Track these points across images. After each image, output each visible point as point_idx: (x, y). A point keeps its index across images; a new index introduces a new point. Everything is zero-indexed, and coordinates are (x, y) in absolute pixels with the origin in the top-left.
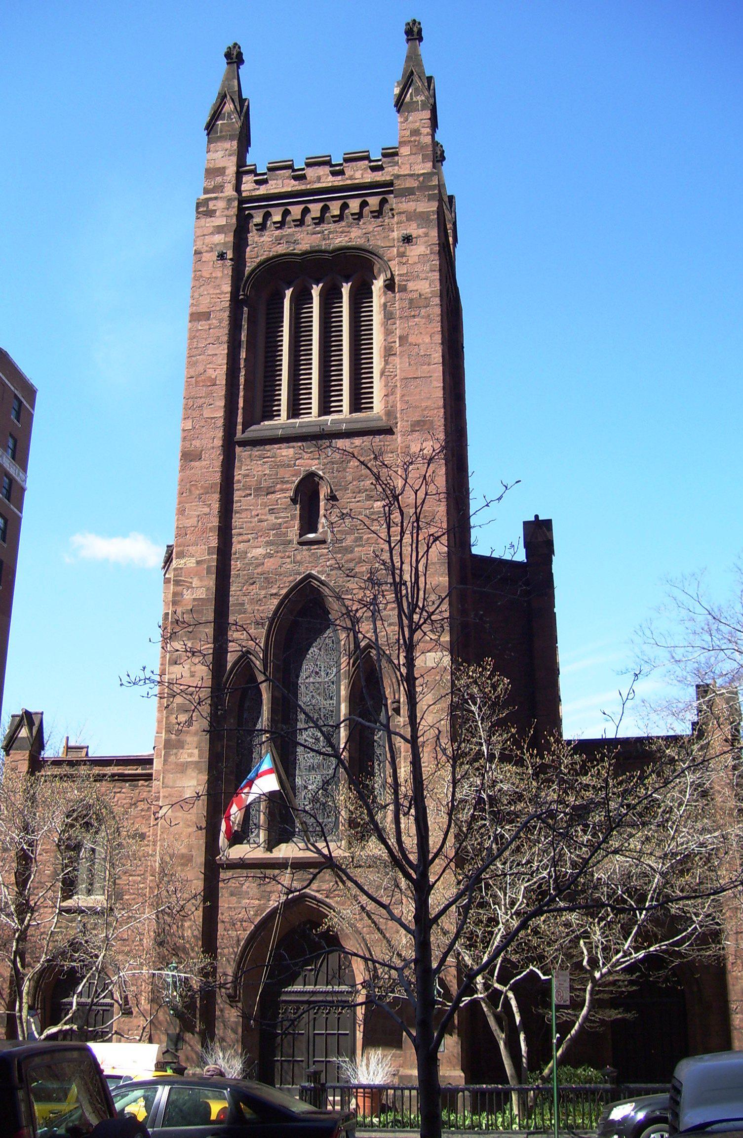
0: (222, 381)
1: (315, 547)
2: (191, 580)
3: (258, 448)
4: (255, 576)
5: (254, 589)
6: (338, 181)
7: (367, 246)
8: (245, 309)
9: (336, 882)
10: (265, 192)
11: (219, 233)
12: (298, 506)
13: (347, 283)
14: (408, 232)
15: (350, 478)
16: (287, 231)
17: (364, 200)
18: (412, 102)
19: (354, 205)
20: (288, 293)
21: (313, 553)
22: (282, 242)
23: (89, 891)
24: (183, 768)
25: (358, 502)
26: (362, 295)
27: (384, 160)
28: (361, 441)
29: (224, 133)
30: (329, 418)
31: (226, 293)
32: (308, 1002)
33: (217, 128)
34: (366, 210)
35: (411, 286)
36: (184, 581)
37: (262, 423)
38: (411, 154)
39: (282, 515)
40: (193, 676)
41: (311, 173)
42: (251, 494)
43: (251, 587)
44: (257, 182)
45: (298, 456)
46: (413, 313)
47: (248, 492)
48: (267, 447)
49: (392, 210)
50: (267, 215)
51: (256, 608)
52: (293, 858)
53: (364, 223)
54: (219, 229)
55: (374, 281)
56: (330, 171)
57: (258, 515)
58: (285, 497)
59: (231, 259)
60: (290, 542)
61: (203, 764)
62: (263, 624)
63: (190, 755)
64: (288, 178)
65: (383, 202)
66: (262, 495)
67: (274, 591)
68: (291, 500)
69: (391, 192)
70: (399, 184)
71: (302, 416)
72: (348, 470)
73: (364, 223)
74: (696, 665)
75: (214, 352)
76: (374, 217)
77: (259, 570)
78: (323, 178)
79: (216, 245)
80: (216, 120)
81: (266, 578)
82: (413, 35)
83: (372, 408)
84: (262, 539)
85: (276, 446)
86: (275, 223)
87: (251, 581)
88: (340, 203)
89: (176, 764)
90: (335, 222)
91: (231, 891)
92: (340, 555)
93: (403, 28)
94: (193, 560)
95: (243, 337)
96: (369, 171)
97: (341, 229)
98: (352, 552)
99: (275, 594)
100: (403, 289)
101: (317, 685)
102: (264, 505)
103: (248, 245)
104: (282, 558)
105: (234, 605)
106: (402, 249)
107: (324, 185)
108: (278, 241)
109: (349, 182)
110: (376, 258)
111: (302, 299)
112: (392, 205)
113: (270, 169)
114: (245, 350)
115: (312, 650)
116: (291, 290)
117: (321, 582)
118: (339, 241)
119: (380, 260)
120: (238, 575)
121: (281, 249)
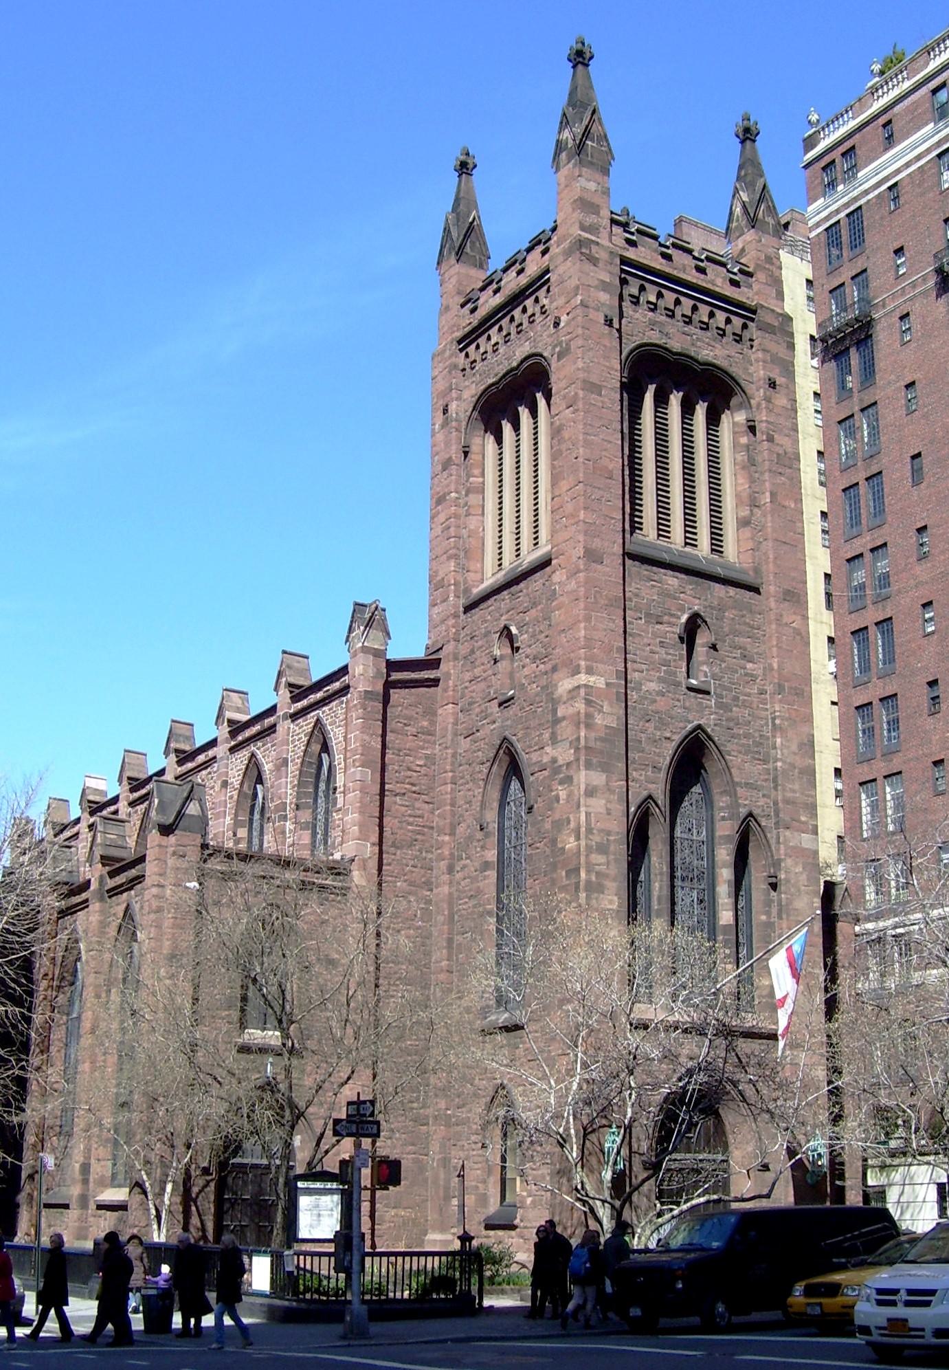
1: (701, 696)
5: (650, 727)
13: (704, 402)
15: (726, 629)
20: (652, 388)
29: (595, 161)
33: (587, 150)
36: (595, 702)
38: (766, 284)
39: (671, 651)
43: (647, 724)
45: (682, 590)
46: (780, 470)
47: (639, 615)
49: (751, 340)
52: (638, 1020)
54: (604, 286)
58: (673, 633)
62: (660, 769)
63: (611, 902)
64: (656, 251)
67: (668, 735)
69: (752, 320)
70: (762, 315)
74: (591, 837)
78: (683, 267)
87: (648, 718)
90: (702, 328)
99: (669, 738)
100: (770, 439)
111: (661, 401)
116: (654, 386)
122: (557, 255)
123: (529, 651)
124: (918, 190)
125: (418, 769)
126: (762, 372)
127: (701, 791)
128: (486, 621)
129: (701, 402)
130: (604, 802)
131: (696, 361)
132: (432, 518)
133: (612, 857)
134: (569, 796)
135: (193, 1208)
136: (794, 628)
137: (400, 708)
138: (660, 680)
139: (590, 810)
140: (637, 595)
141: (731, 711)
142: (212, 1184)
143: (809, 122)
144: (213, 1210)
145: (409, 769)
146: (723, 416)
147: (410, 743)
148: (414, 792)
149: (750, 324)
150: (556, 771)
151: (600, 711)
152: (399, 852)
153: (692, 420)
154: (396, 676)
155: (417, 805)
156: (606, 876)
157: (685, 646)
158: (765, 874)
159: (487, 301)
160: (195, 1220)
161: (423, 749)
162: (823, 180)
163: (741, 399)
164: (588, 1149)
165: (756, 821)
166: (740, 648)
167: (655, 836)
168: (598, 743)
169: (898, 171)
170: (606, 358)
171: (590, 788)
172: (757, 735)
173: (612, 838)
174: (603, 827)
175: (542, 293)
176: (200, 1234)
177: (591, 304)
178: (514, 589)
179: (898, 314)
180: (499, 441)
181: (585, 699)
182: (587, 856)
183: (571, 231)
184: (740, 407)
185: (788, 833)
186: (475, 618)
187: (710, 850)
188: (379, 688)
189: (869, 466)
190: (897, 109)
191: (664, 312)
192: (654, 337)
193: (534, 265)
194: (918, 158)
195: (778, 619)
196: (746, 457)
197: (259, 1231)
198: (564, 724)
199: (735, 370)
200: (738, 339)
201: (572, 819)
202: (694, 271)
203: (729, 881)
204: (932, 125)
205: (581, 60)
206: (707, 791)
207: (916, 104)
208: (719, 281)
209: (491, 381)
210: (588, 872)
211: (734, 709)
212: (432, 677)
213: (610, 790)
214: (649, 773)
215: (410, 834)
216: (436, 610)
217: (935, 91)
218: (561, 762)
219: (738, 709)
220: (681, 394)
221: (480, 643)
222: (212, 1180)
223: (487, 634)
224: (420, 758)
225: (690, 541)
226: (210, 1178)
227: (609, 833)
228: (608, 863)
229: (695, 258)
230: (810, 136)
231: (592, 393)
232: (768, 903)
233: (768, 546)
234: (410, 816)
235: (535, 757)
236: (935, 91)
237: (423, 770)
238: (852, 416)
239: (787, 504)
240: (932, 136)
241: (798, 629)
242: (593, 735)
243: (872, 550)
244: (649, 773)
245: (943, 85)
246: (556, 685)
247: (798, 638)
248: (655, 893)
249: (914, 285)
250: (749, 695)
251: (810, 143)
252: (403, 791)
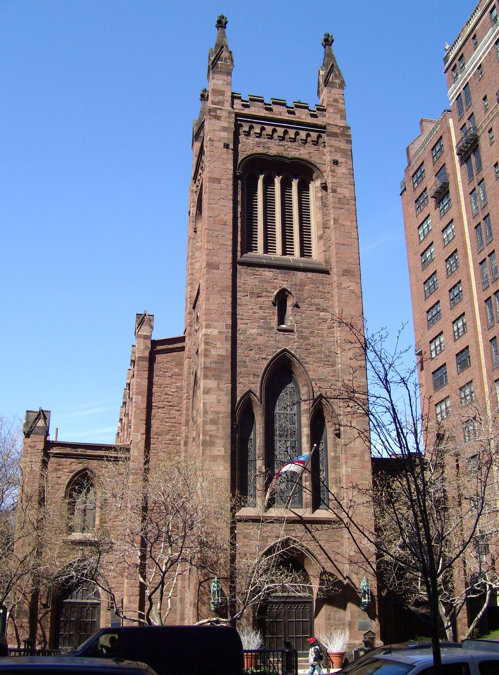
0: (230, 222)
1: (287, 333)
2: (215, 343)
3: (251, 268)
4: (252, 345)
6: (291, 117)
7: (310, 160)
8: (239, 182)
9: (306, 532)
10: (248, 113)
11: (224, 131)
12: (276, 307)
14: (335, 158)
15: (306, 296)
16: (262, 140)
17: (286, 130)
18: (333, 83)
19: (303, 134)
20: (261, 177)
21: (286, 337)
22: (260, 145)
23: (84, 529)
24: (214, 458)
25: (311, 310)
26: (303, 188)
27: (317, 111)
28: (311, 275)
29: (223, 70)
30: (287, 257)
31: (230, 169)
32: (285, 603)
33: (218, 65)
34: (309, 139)
35: (339, 190)
37: (248, 253)
38: (334, 113)
39: (267, 311)
40: (219, 402)
41: (275, 108)
42: (247, 296)
43: (250, 352)
44: (243, 105)
45: (275, 278)
46: (341, 207)
47: (246, 294)
48: (257, 269)
50: (251, 127)
51: (254, 365)
53: (308, 147)
54: (224, 129)
55: (311, 182)
56: (288, 110)
57: (252, 309)
58: (269, 301)
59: (232, 149)
60: (272, 328)
61: (228, 457)
62: (259, 376)
63: (219, 451)
64: (262, 107)
65: (319, 137)
66: (255, 297)
67: (264, 356)
68: (273, 303)
69: (324, 132)
70: (329, 129)
71: (269, 253)
72: (305, 291)
73: (308, 147)
75: (223, 204)
76: (313, 144)
77: (255, 342)
78: (280, 112)
79: (223, 138)
80: (217, 61)
81: (259, 348)
82: (328, 42)
83: (311, 256)
84: (255, 324)
85: (262, 269)
86: (256, 133)
87: (250, 348)
88: (284, 129)
89: (211, 456)
90: (291, 141)
91: (244, 536)
92: (302, 341)
93: (217, 19)
94: (216, 331)
95: (239, 199)
96: (309, 116)
97: (295, 147)
98: (309, 339)
99: (265, 358)
100: (334, 191)
101: (286, 415)
102: (256, 303)
103: (239, 143)
104: (268, 337)
105: (239, 361)
106: (333, 168)
107: (284, 118)
108: (258, 144)
109: (298, 120)
110: (316, 169)
111: (269, 183)
112: (324, 140)
113: (250, 99)
114: (240, 207)
115: (282, 394)
116: (263, 175)
117: (292, 355)
118: (293, 154)
119: (318, 171)
120: (242, 344)
121: (260, 150)
124: (489, 64)
125: (172, 394)
126: (329, 157)
127: (293, 386)
129: (294, 180)
130: (215, 396)
131: (287, 158)
133: (220, 426)
135: (39, 625)
136: (351, 290)
137: (162, 364)
138: (260, 327)
139: (205, 401)
140: (244, 284)
141: (309, 339)
142: (50, 613)
143: (445, 49)
144: (49, 626)
145: (166, 394)
146: (310, 185)
147: (168, 381)
148: (170, 406)
149: (323, 135)
152: (160, 437)
153: (308, 193)
154: (159, 348)
155: (171, 412)
156: (217, 437)
157: (276, 307)
158: (333, 429)
160: (39, 631)
161: (176, 383)
162: (453, 75)
163: (317, 174)
164: (201, 591)
165: (254, 394)
166: (315, 305)
167: (257, 413)
168: (213, 365)
170: (225, 164)
171: (206, 389)
173: (221, 416)
174: (215, 410)
176: (42, 639)
177: (215, 139)
179: (488, 130)
181: (204, 342)
182: (203, 427)
184: (317, 178)
187: (299, 419)
188: (147, 354)
189: (483, 212)
191: (266, 137)
194: (488, 48)
195: (339, 286)
196: (321, 203)
197: (80, 637)
199: (313, 160)
200: (316, 143)
202: (287, 114)
204: (492, 28)
205: (220, 25)
206: (297, 385)
208: (303, 117)
210: (204, 435)
211: (311, 338)
212: (180, 346)
213: (220, 389)
214: (251, 379)
215: (167, 428)
217: (491, 12)
219: (313, 338)
220: (298, 180)
222: (49, 611)
224: (173, 388)
226: (48, 609)
227: (219, 413)
228: (218, 430)
229: (287, 107)
230: (446, 56)
231: (214, 183)
232: (335, 445)
233: (333, 249)
234: (167, 418)
236: (491, 12)
237: (175, 394)
238: (474, 189)
239: (345, 224)
240: (492, 35)
241: (353, 290)
242: (209, 360)
243: (489, 255)
244: (251, 379)
245: (494, 7)
247: (353, 295)
248: (257, 445)
250: (322, 330)
251: (446, 59)
252: (163, 406)
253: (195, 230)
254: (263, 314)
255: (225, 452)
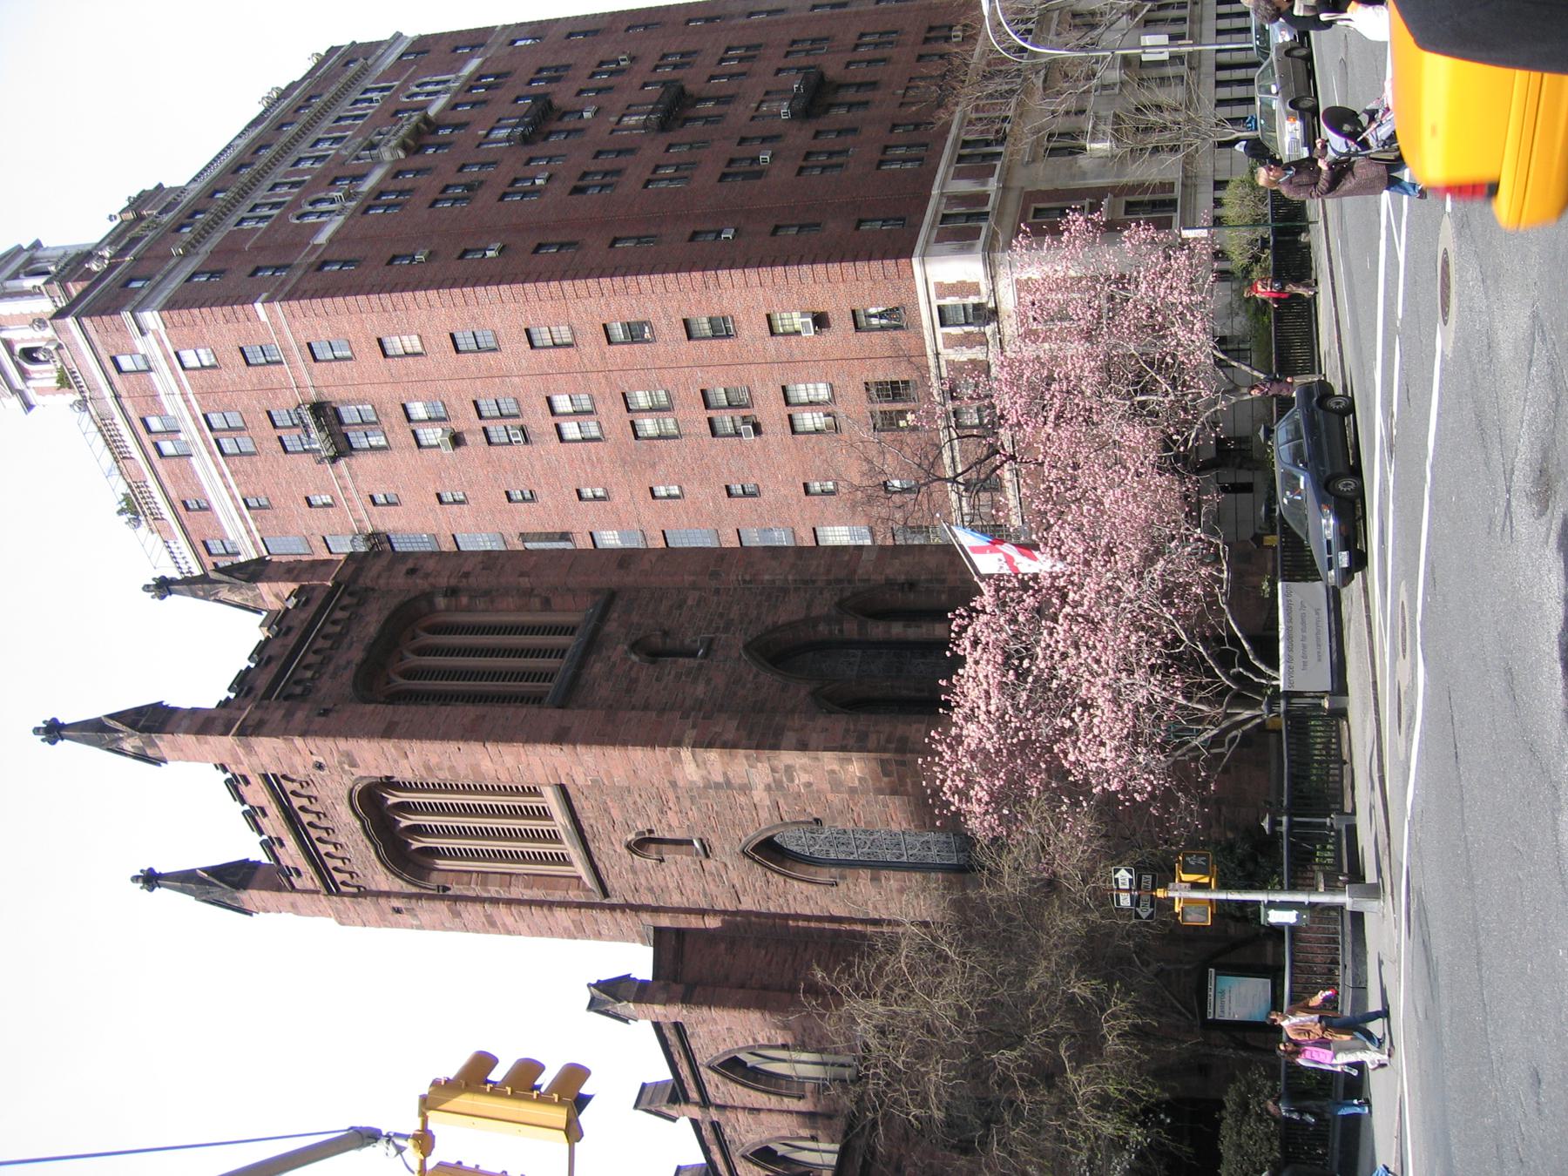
100: (466, 575)
122: (250, 765)
123: (654, 818)
128: (620, 872)
132: (509, 932)
134: (806, 771)
148: (794, 960)
150: (779, 784)
151: (720, 734)
159: (291, 856)
169: (233, 498)
172: (759, 598)
175: (288, 786)
178: (589, 836)
180: (434, 853)
183: (229, 746)
185: (860, 571)
186: (616, 886)
190: (173, 494)
192: (347, 676)
193: (258, 794)
194: (222, 475)
198: (731, 775)
199: (394, 602)
201: (830, 767)
203: (905, 626)
207: (171, 474)
209: (373, 856)
216: (605, 931)
218: (770, 779)
221: (643, 881)
223: (633, 870)
225: (561, 653)
227: (847, 731)
228: (878, 732)
235: (764, 815)
246: (691, 782)
249: (344, 488)
250: (718, 604)
253: (618, 332)
254: (671, 677)
255: (922, 723)
